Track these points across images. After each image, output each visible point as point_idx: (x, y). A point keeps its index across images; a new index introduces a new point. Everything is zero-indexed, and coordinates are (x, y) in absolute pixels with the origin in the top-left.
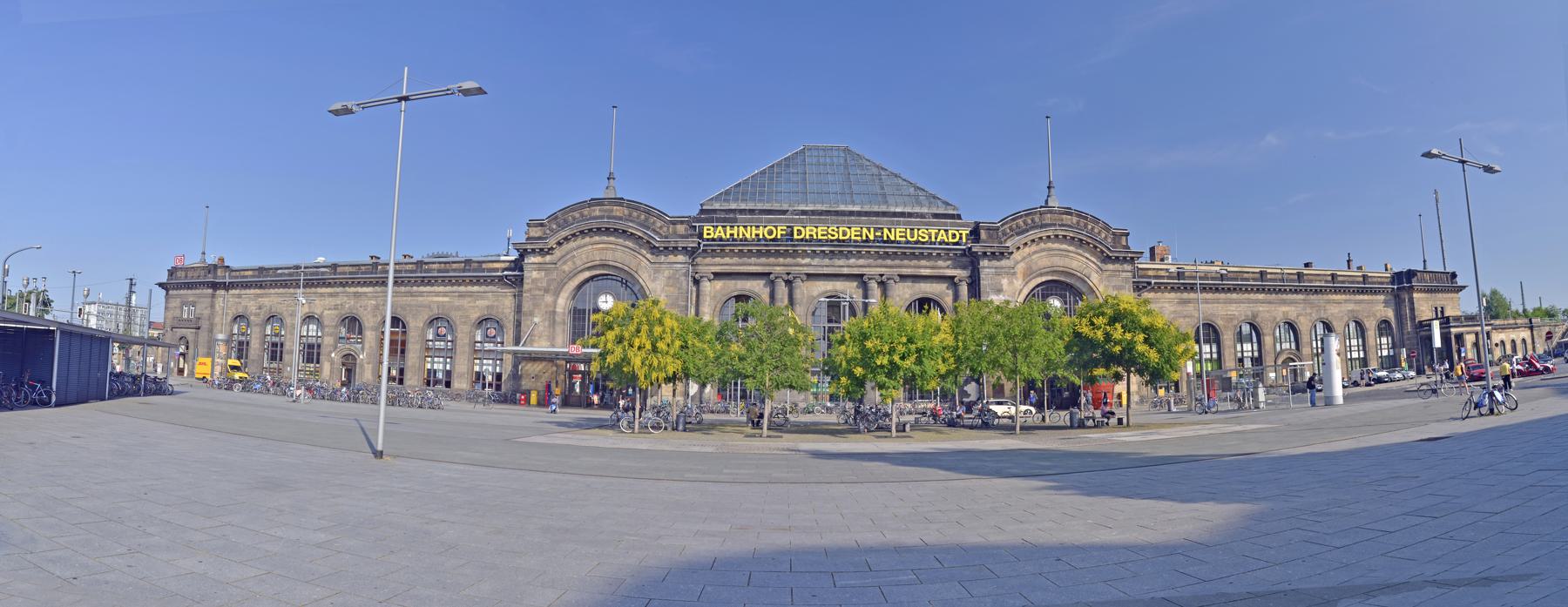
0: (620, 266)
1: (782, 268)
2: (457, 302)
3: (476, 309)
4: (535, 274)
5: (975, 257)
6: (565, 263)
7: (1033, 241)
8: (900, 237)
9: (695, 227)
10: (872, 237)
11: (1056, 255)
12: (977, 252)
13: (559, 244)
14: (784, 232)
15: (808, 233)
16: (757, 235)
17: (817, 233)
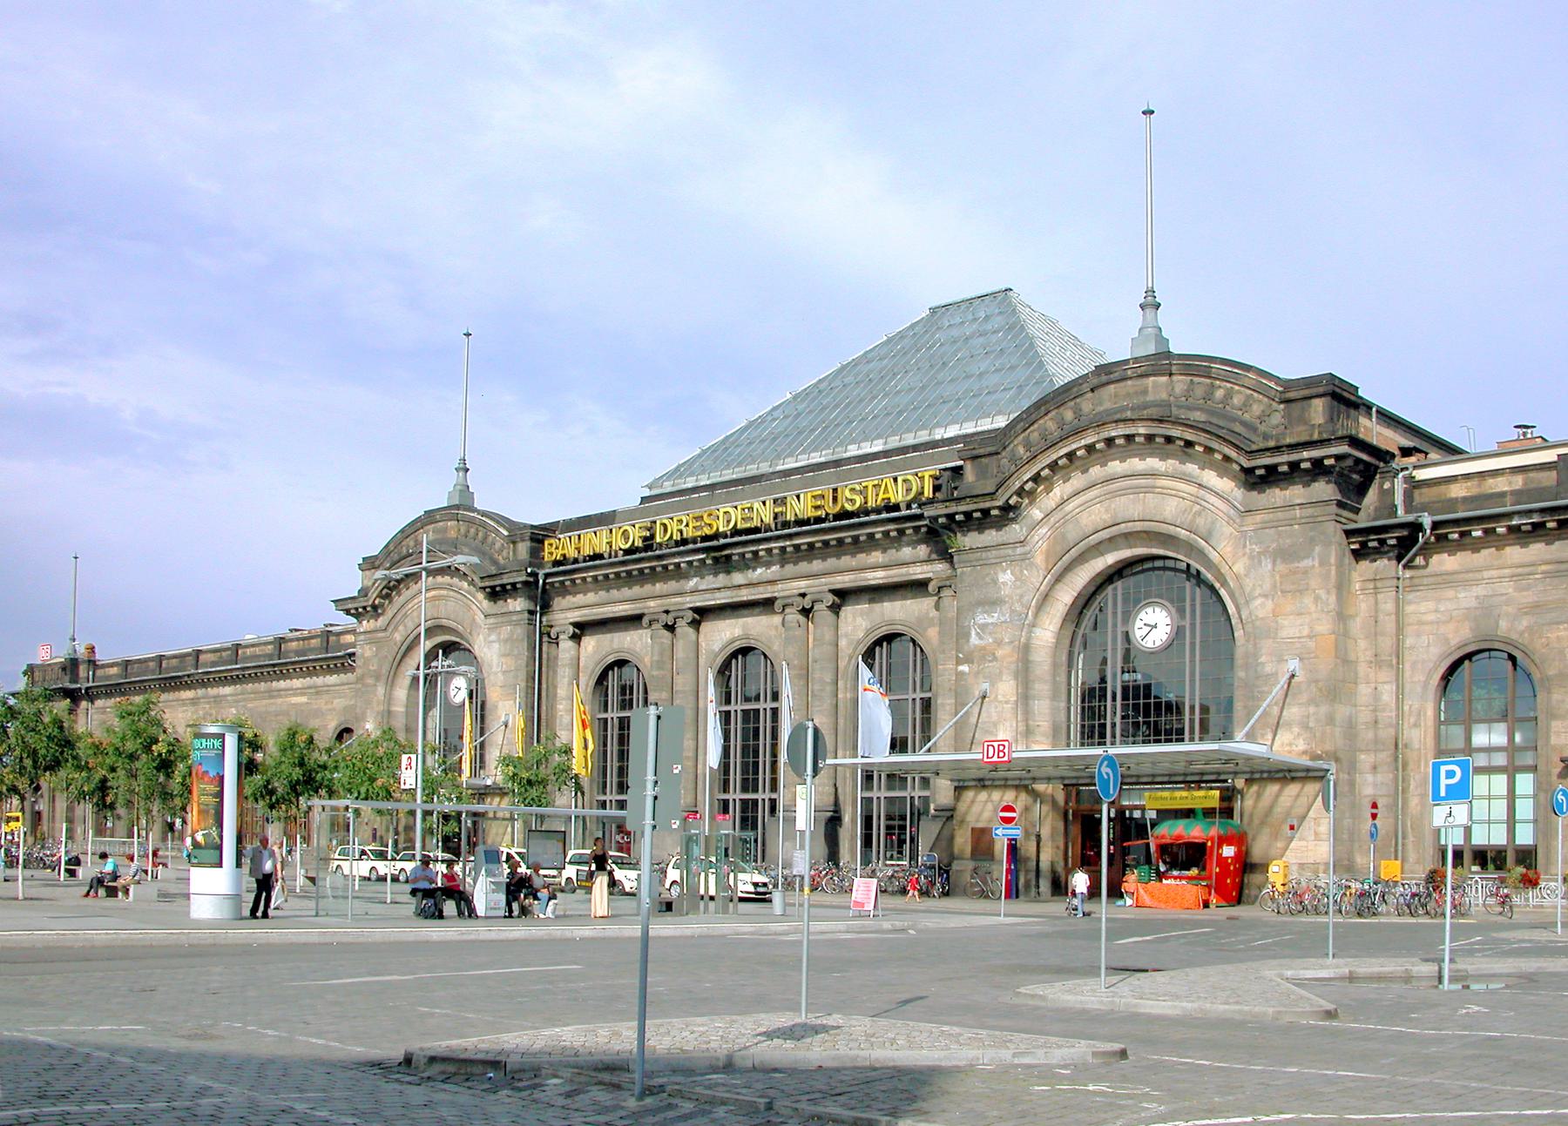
1: (659, 602)
11: (1123, 492)
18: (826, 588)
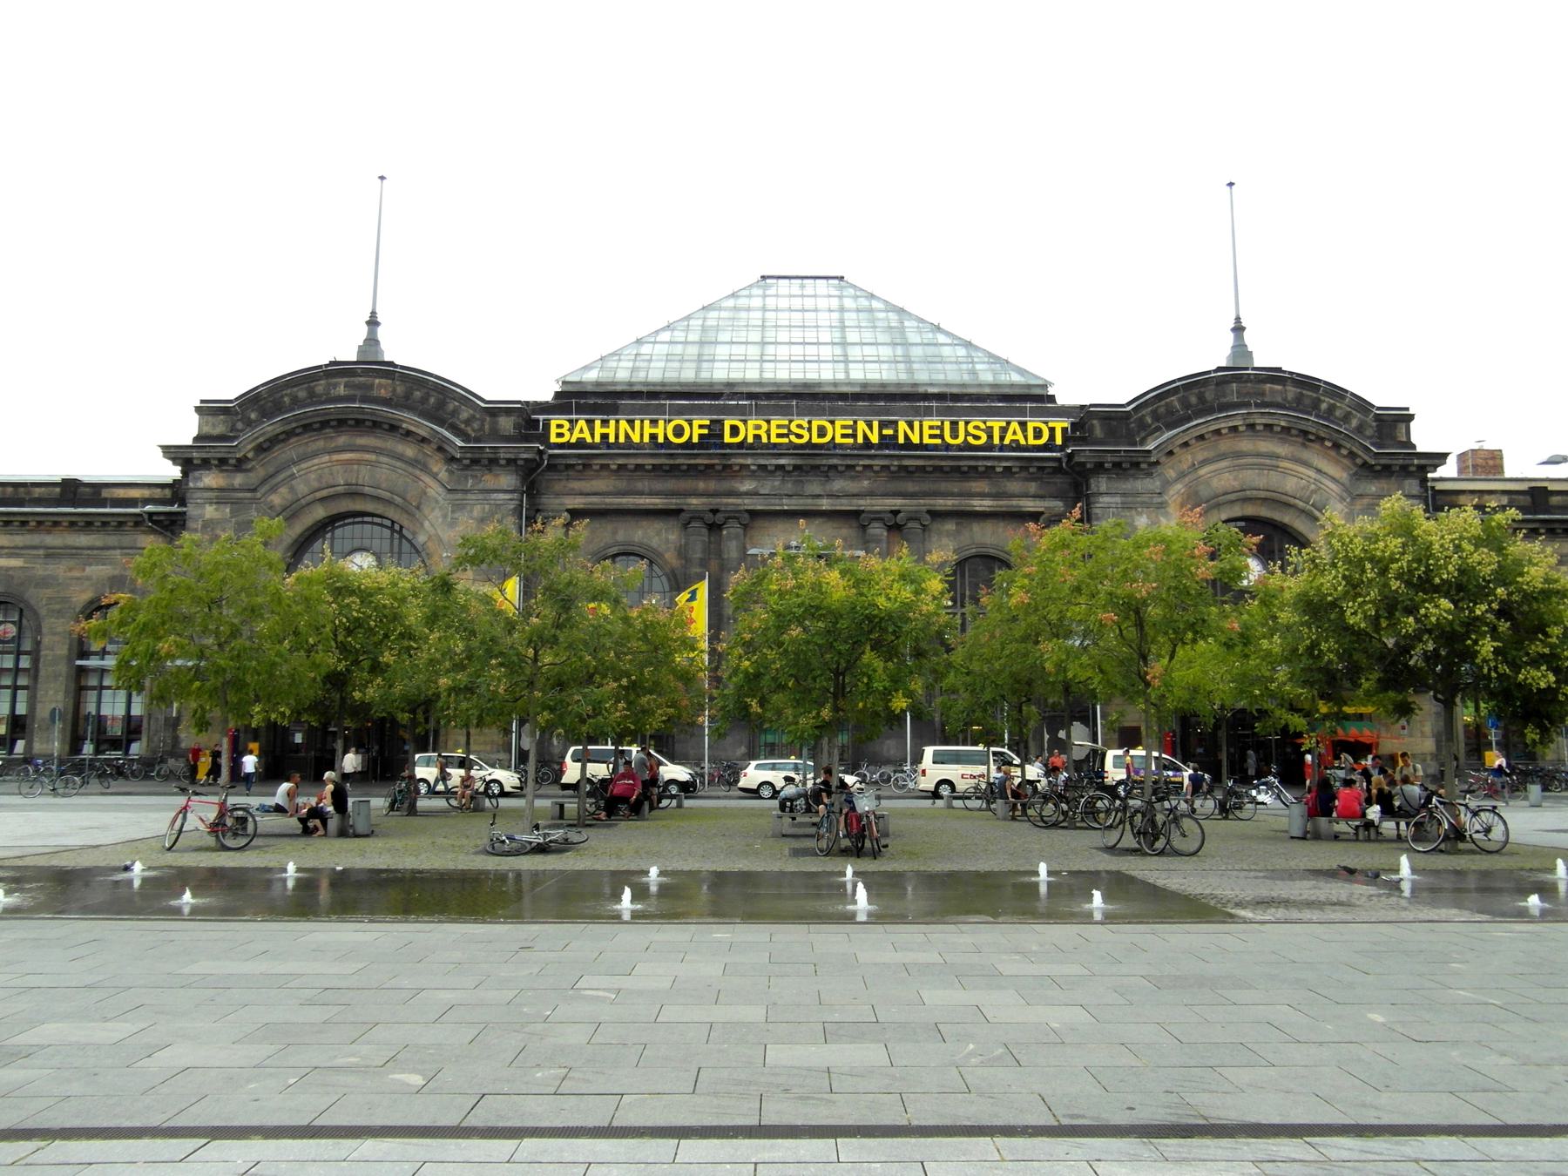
0: (387, 495)
1: (704, 500)
2: (41, 570)
3: (87, 583)
4: (210, 511)
5: (1079, 473)
6: (274, 489)
7: (1201, 437)
8: (931, 436)
9: (538, 421)
10: (875, 439)
12: (1083, 464)
13: (261, 449)
14: (705, 431)
15: (751, 433)
16: (653, 437)
17: (768, 433)
18: (925, 508)
